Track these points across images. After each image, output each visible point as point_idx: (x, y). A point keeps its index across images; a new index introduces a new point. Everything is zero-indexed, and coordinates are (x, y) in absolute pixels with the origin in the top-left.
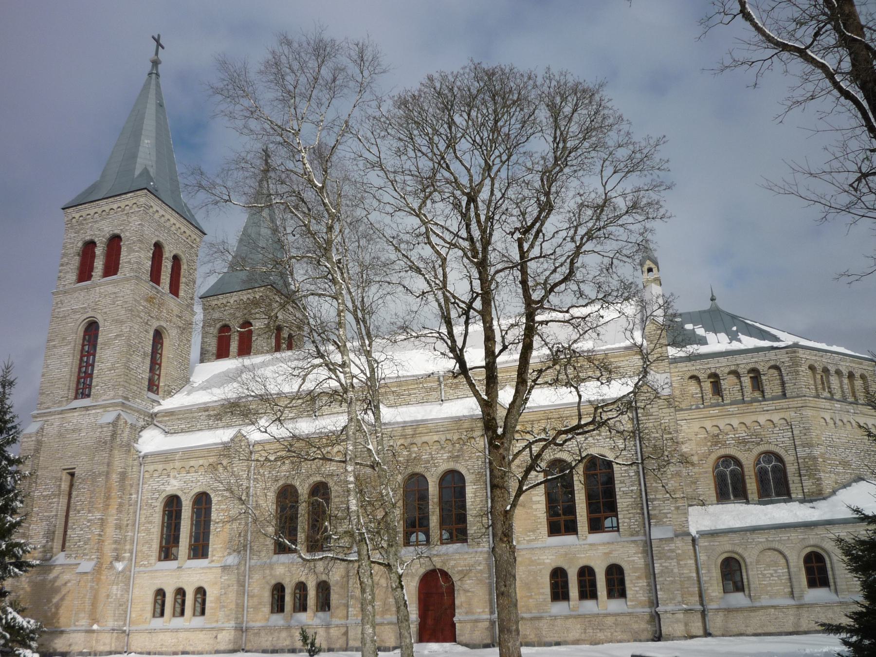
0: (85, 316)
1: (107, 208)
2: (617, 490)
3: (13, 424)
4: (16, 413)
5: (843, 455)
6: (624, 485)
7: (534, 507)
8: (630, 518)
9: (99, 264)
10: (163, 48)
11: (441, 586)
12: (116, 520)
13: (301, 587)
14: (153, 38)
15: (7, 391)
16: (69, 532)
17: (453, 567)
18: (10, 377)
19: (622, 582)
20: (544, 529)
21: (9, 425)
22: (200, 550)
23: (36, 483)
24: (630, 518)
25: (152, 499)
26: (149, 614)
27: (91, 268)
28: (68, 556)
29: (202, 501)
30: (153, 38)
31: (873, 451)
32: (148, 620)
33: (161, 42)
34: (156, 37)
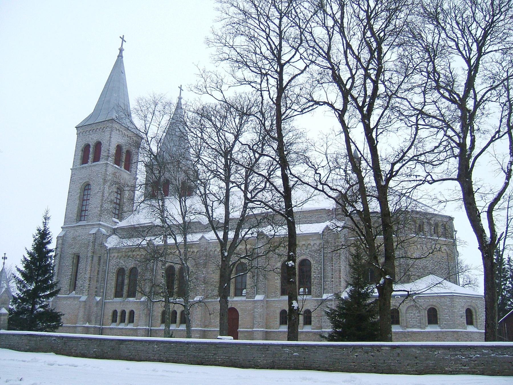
0: (85, 181)
1: (95, 128)
2: (312, 276)
3: (49, 236)
4: (50, 231)
5: (425, 264)
6: (315, 274)
7: (276, 281)
8: (316, 289)
9: (91, 156)
10: (125, 42)
11: (13, 309)
12: (97, 278)
13: (123, 313)
14: (120, 37)
15: (47, 222)
16: (77, 282)
17: (239, 307)
18: (48, 216)
19: (310, 317)
20: (279, 292)
21: (48, 236)
22: (131, 293)
23: (63, 259)
24: (316, 289)
25: (112, 269)
26: (110, 321)
27: (88, 158)
28: (76, 293)
29: (133, 271)
30: (120, 37)
31: (443, 262)
32: (110, 324)
33: (124, 39)
34: (122, 37)
